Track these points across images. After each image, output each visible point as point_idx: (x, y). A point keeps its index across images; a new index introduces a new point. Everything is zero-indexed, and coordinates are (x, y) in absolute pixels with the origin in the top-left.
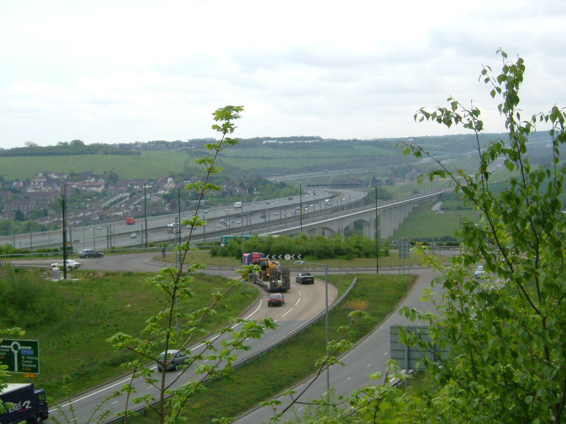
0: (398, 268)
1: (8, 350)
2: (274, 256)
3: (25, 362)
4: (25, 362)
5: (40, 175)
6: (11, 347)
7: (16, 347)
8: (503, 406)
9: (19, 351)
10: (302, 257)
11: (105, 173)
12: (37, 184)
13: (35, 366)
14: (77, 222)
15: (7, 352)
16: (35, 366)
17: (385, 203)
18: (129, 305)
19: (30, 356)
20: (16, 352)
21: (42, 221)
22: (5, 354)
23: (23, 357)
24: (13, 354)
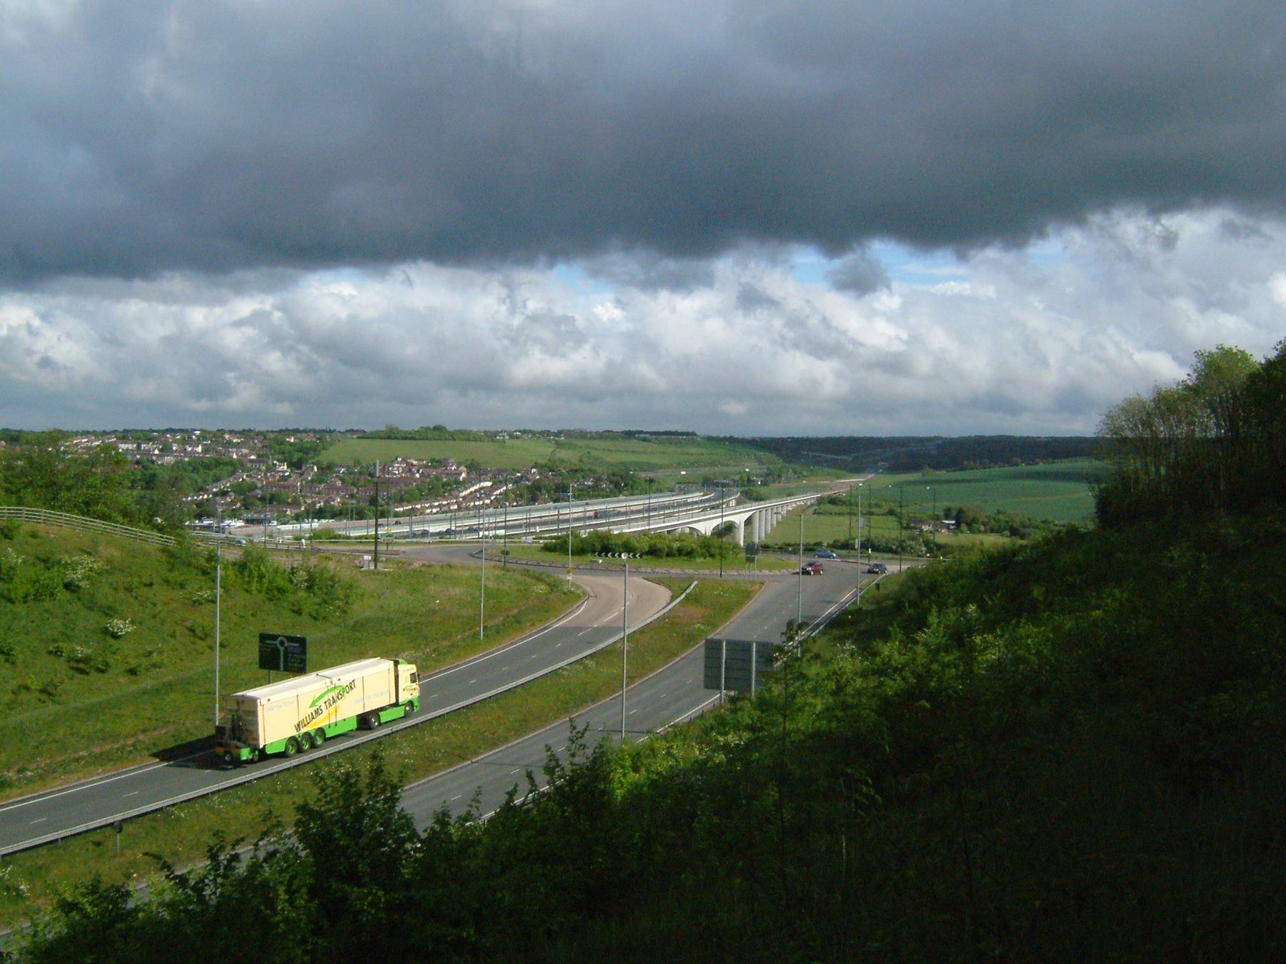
0: (561, 517)
1: (274, 646)
2: (610, 554)
3: (292, 660)
4: (292, 660)
5: (400, 459)
6: (277, 642)
7: (282, 643)
8: (895, 515)
9: (286, 648)
10: (641, 556)
11: (467, 460)
12: (395, 469)
13: (302, 666)
14: (434, 511)
15: (272, 649)
16: (302, 666)
17: (757, 503)
18: (438, 601)
19: (298, 654)
20: (282, 649)
21: (109, 439)
22: (269, 650)
23: (290, 655)
24: (279, 650)
